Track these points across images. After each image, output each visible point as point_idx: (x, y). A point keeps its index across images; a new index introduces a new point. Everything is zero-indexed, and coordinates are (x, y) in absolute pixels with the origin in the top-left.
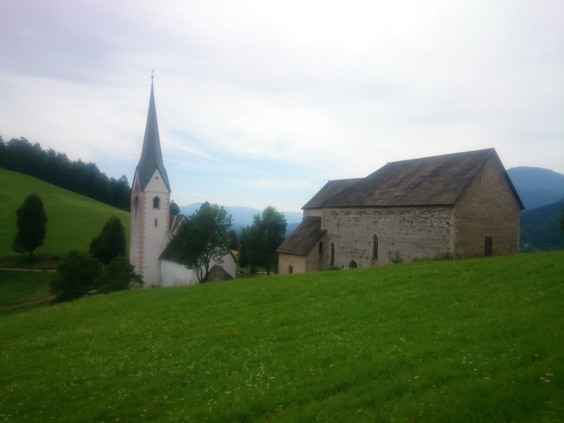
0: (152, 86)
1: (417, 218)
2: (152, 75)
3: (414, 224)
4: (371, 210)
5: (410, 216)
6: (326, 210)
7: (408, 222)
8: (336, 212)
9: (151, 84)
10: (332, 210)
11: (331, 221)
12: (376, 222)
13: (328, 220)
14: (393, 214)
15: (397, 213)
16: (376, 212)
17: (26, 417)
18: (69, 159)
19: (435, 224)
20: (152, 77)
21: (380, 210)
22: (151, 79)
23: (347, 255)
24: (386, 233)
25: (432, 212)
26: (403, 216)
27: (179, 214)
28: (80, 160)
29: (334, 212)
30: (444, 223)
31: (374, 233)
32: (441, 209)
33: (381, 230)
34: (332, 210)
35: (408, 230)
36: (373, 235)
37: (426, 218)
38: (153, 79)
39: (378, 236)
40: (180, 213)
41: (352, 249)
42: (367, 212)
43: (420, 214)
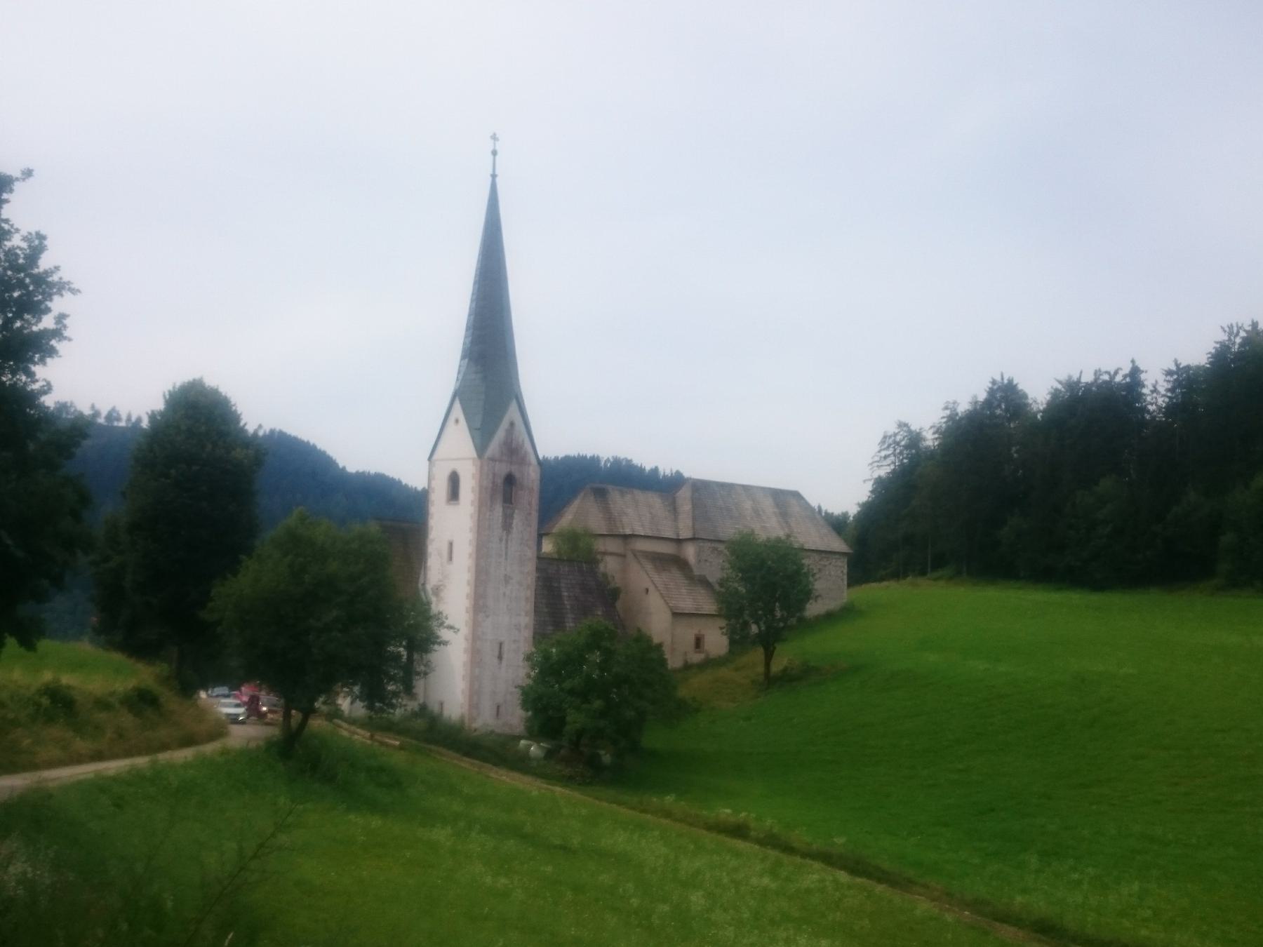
0: (494, 176)
2: (492, 149)
6: (702, 544)
8: (719, 549)
10: (713, 545)
11: (711, 562)
13: (706, 561)
18: (601, 455)
19: (833, 573)
20: (494, 153)
22: (492, 157)
28: (47, 249)
29: (715, 549)
30: (839, 572)
32: (837, 556)
34: (713, 545)
37: (825, 566)
38: (497, 157)
43: (820, 560)
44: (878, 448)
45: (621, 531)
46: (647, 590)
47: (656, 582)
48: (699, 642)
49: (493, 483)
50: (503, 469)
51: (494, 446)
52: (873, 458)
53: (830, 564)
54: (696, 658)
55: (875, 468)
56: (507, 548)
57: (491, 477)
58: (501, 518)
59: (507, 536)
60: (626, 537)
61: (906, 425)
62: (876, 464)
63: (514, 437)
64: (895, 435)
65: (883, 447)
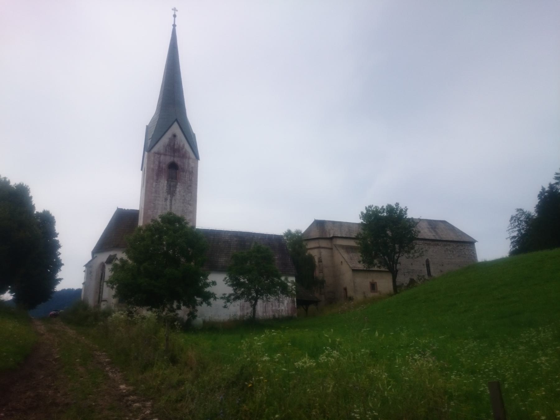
0: (174, 26)
1: (455, 249)
3: (454, 253)
4: (420, 242)
5: (451, 248)
7: (450, 251)
9: (173, 23)
12: (426, 250)
14: (439, 246)
15: (441, 246)
16: (426, 243)
17: (134, 401)
20: (175, 16)
21: (428, 242)
22: (173, 18)
23: (404, 275)
24: (436, 258)
25: (464, 246)
26: (446, 247)
27: (9, 291)
31: (427, 258)
33: (432, 256)
35: (451, 256)
36: (426, 259)
39: (430, 260)
40: (8, 293)
41: (409, 270)
42: (418, 243)
43: (457, 247)
44: (509, 223)
45: (328, 236)
46: (342, 262)
47: (344, 257)
48: (373, 286)
49: (159, 166)
50: (168, 159)
51: (159, 147)
52: (508, 227)
53: (464, 248)
54: (371, 295)
55: (511, 233)
56: (171, 205)
57: (157, 163)
58: (165, 187)
59: (172, 197)
60: (331, 239)
61: (521, 210)
62: (511, 230)
63: (176, 143)
64: (517, 215)
65: (512, 222)
